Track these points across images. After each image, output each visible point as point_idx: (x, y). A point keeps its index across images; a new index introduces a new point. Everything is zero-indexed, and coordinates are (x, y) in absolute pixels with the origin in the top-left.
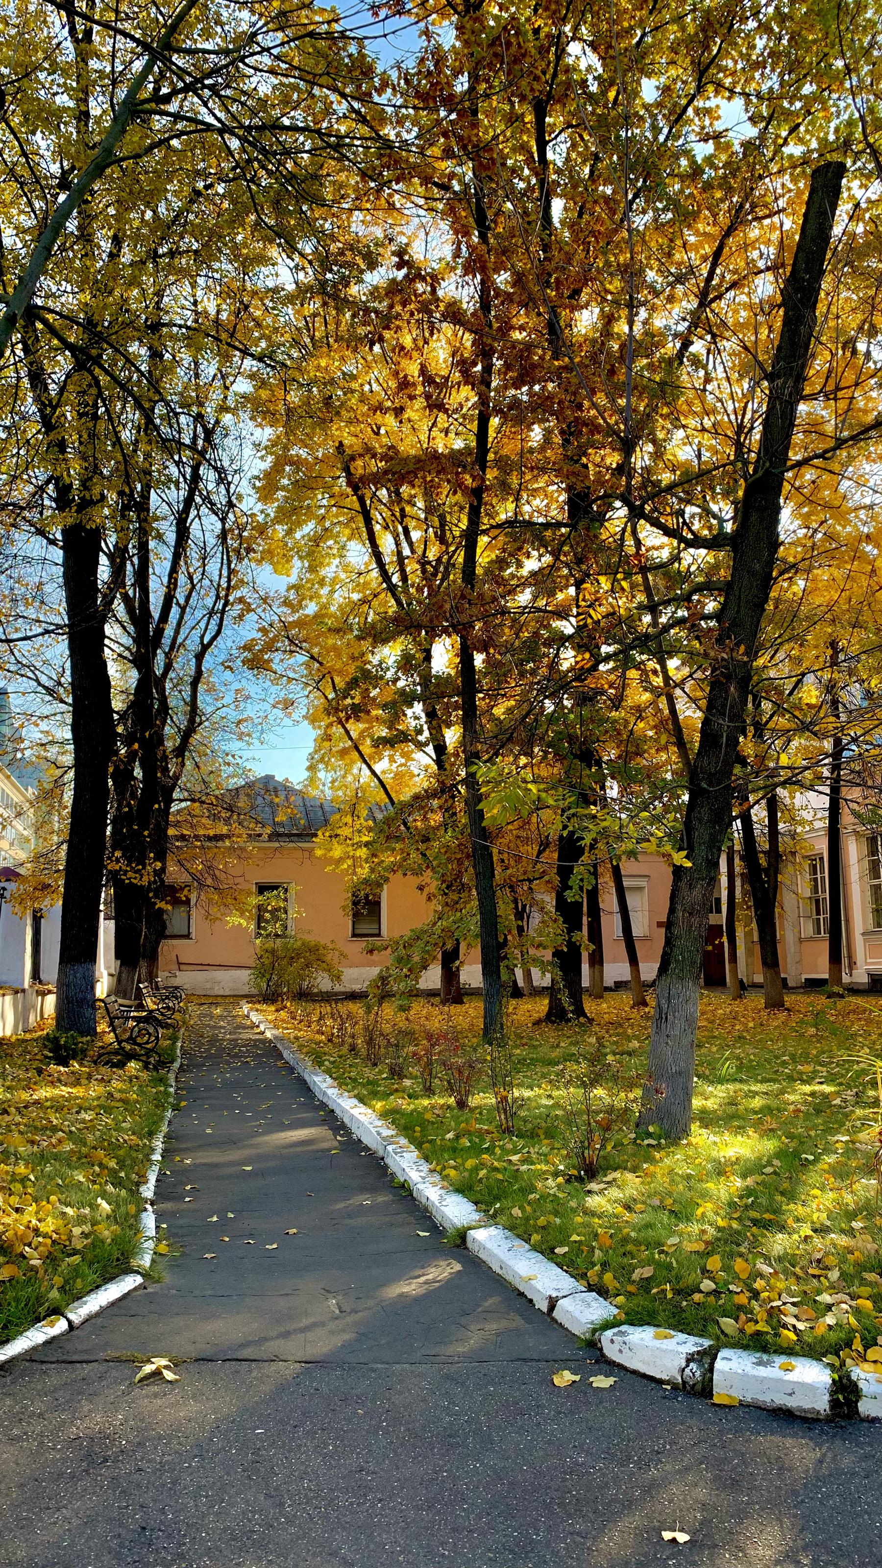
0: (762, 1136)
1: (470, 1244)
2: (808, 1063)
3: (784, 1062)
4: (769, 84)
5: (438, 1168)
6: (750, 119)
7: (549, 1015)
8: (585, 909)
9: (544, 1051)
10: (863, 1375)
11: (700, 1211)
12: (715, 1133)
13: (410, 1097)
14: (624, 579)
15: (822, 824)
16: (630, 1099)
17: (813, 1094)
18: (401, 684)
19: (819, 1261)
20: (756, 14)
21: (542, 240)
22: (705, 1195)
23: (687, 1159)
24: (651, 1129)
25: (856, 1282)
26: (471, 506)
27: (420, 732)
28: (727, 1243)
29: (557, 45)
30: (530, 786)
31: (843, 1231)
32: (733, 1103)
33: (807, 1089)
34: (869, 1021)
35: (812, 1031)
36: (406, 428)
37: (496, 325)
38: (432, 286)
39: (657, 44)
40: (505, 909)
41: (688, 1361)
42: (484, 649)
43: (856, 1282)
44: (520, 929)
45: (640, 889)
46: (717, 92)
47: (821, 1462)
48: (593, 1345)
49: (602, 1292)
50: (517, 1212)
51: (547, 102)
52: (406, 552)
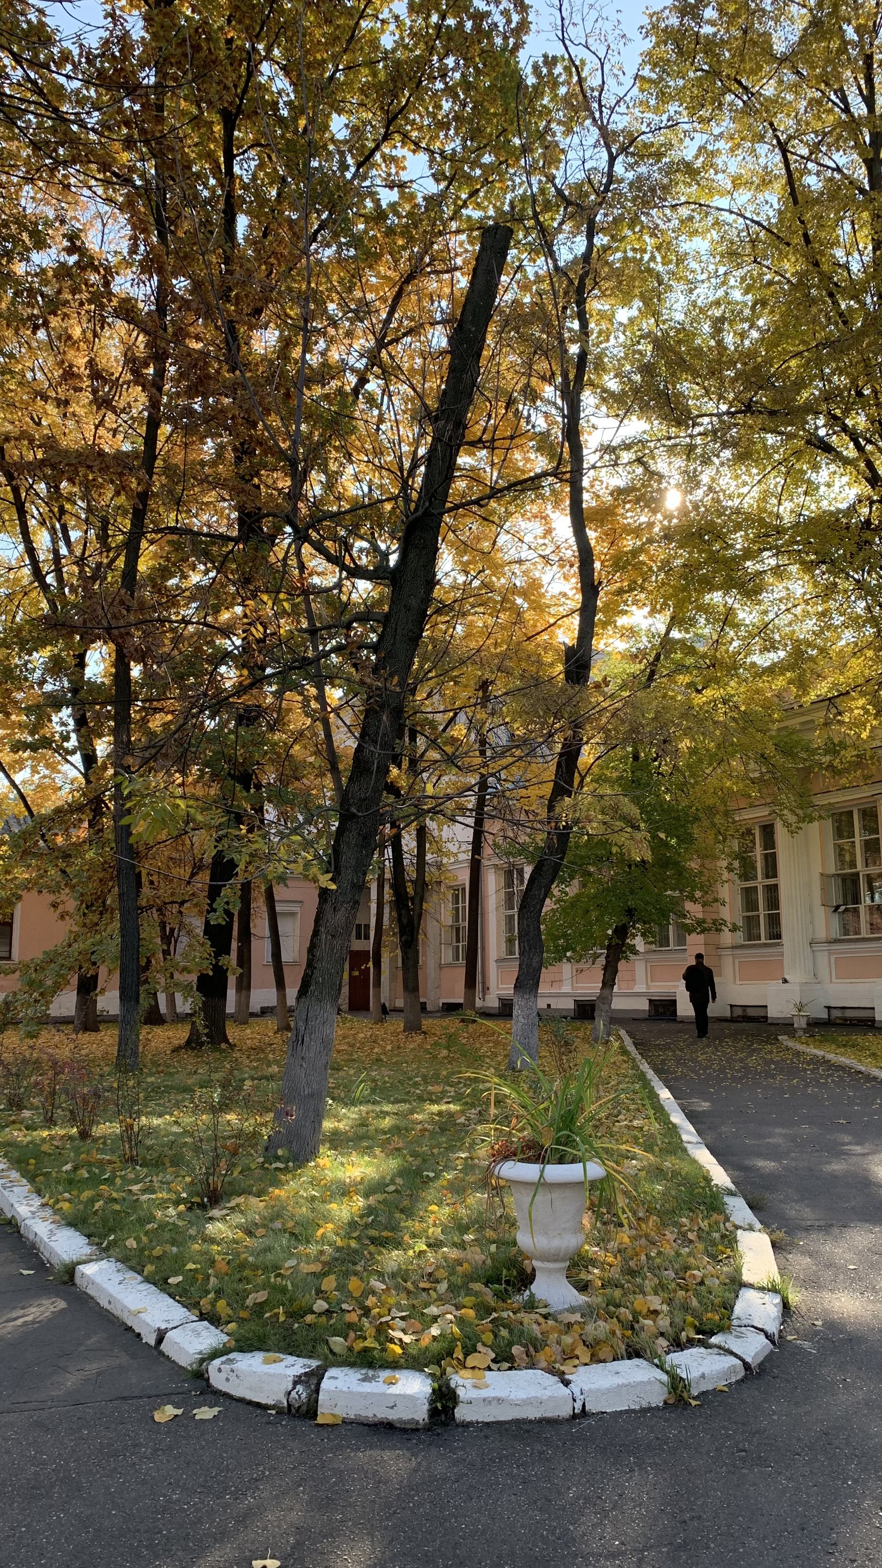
0: (388, 1156)
1: (78, 1280)
2: (438, 1084)
3: (416, 1083)
4: (452, 145)
5: (51, 1202)
6: (433, 175)
7: (188, 1042)
8: (235, 933)
9: (181, 1078)
10: (461, 1382)
11: (321, 1231)
12: (342, 1155)
13: (28, 1128)
14: (287, 600)
15: (466, 857)
16: (263, 1124)
17: (440, 1113)
18: (48, 688)
19: (430, 1275)
20: (444, 76)
21: (225, 252)
22: (327, 1218)
23: (314, 1182)
24: (280, 1152)
25: (462, 1293)
26: (135, 509)
27: (66, 738)
28: (344, 1262)
29: (249, 60)
30: (178, 801)
31: (455, 1245)
32: (363, 1123)
33: (435, 1108)
34: (497, 1043)
35: (445, 1052)
36: (70, 423)
37: (170, 330)
38: (104, 277)
39: (348, 84)
40: (150, 932)
41: (295, 1383)
42: (141, 658)
43: (462, 1293)
44: (166, 953)
45: (292, 914)
46: (404, 144)
47: (415, 1471)
48: (199, 1376)
49: (214, 1319)
50: (131, 1243)
51: (237, 115)
52: (64, 551)
